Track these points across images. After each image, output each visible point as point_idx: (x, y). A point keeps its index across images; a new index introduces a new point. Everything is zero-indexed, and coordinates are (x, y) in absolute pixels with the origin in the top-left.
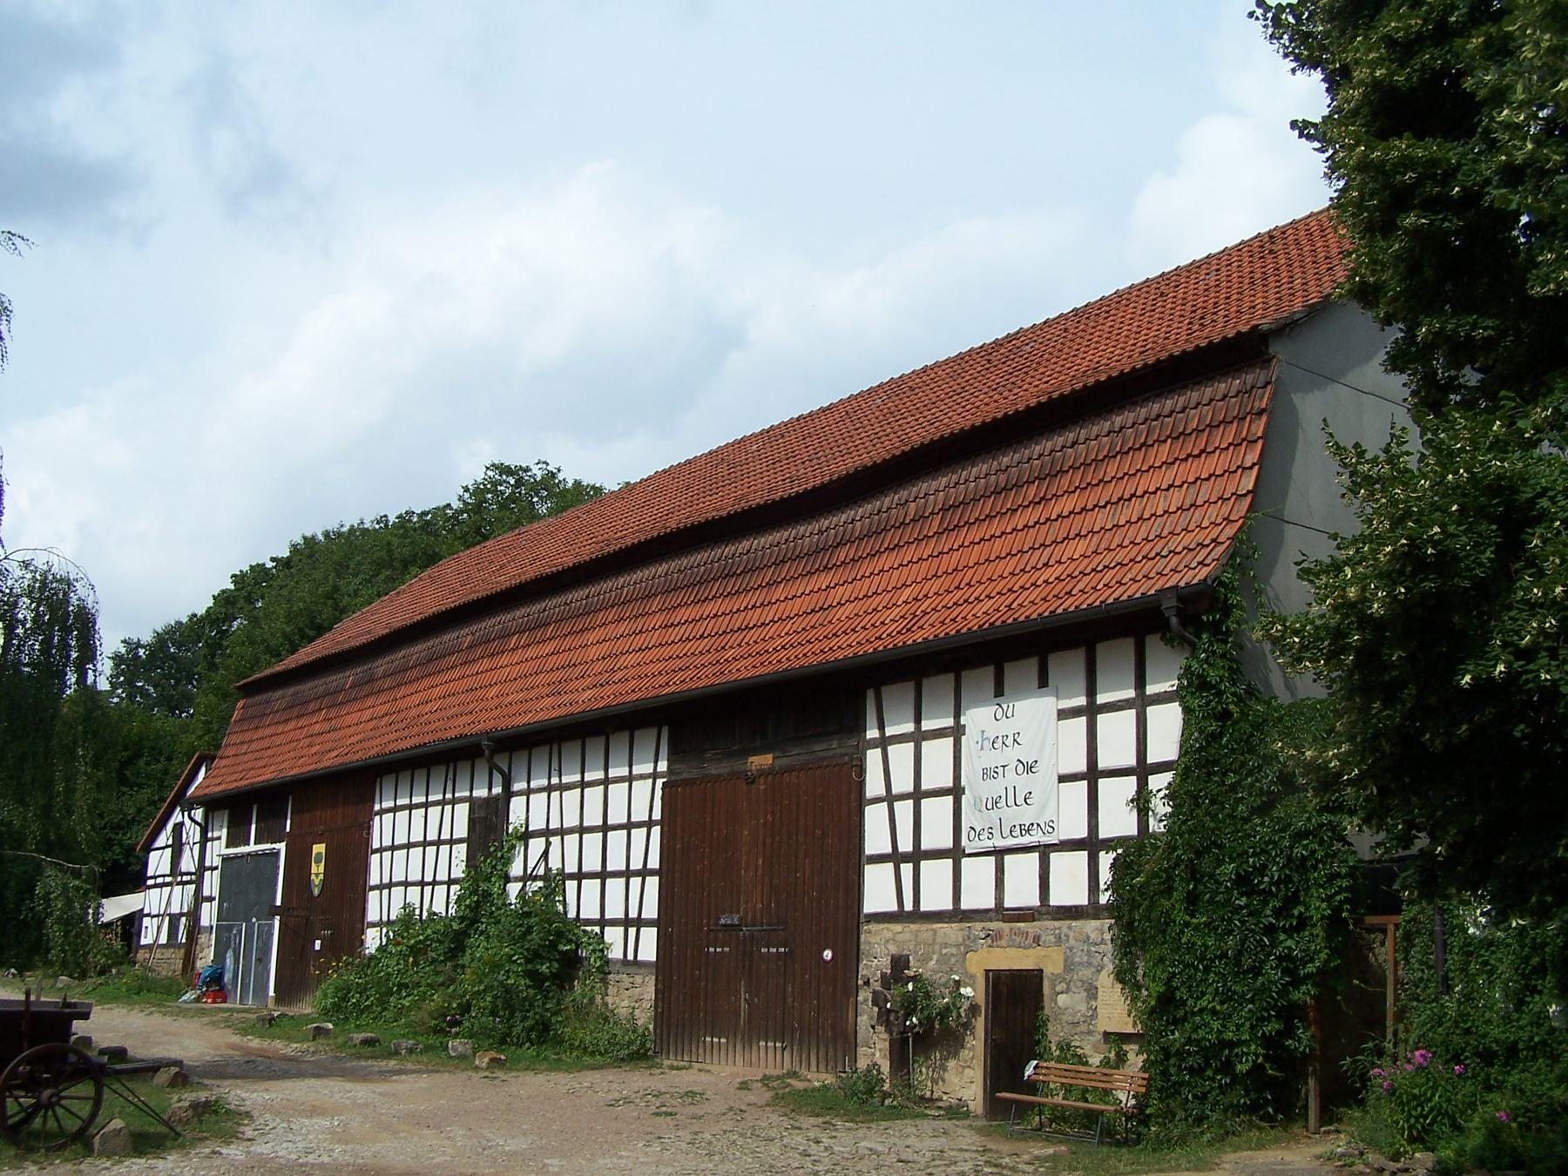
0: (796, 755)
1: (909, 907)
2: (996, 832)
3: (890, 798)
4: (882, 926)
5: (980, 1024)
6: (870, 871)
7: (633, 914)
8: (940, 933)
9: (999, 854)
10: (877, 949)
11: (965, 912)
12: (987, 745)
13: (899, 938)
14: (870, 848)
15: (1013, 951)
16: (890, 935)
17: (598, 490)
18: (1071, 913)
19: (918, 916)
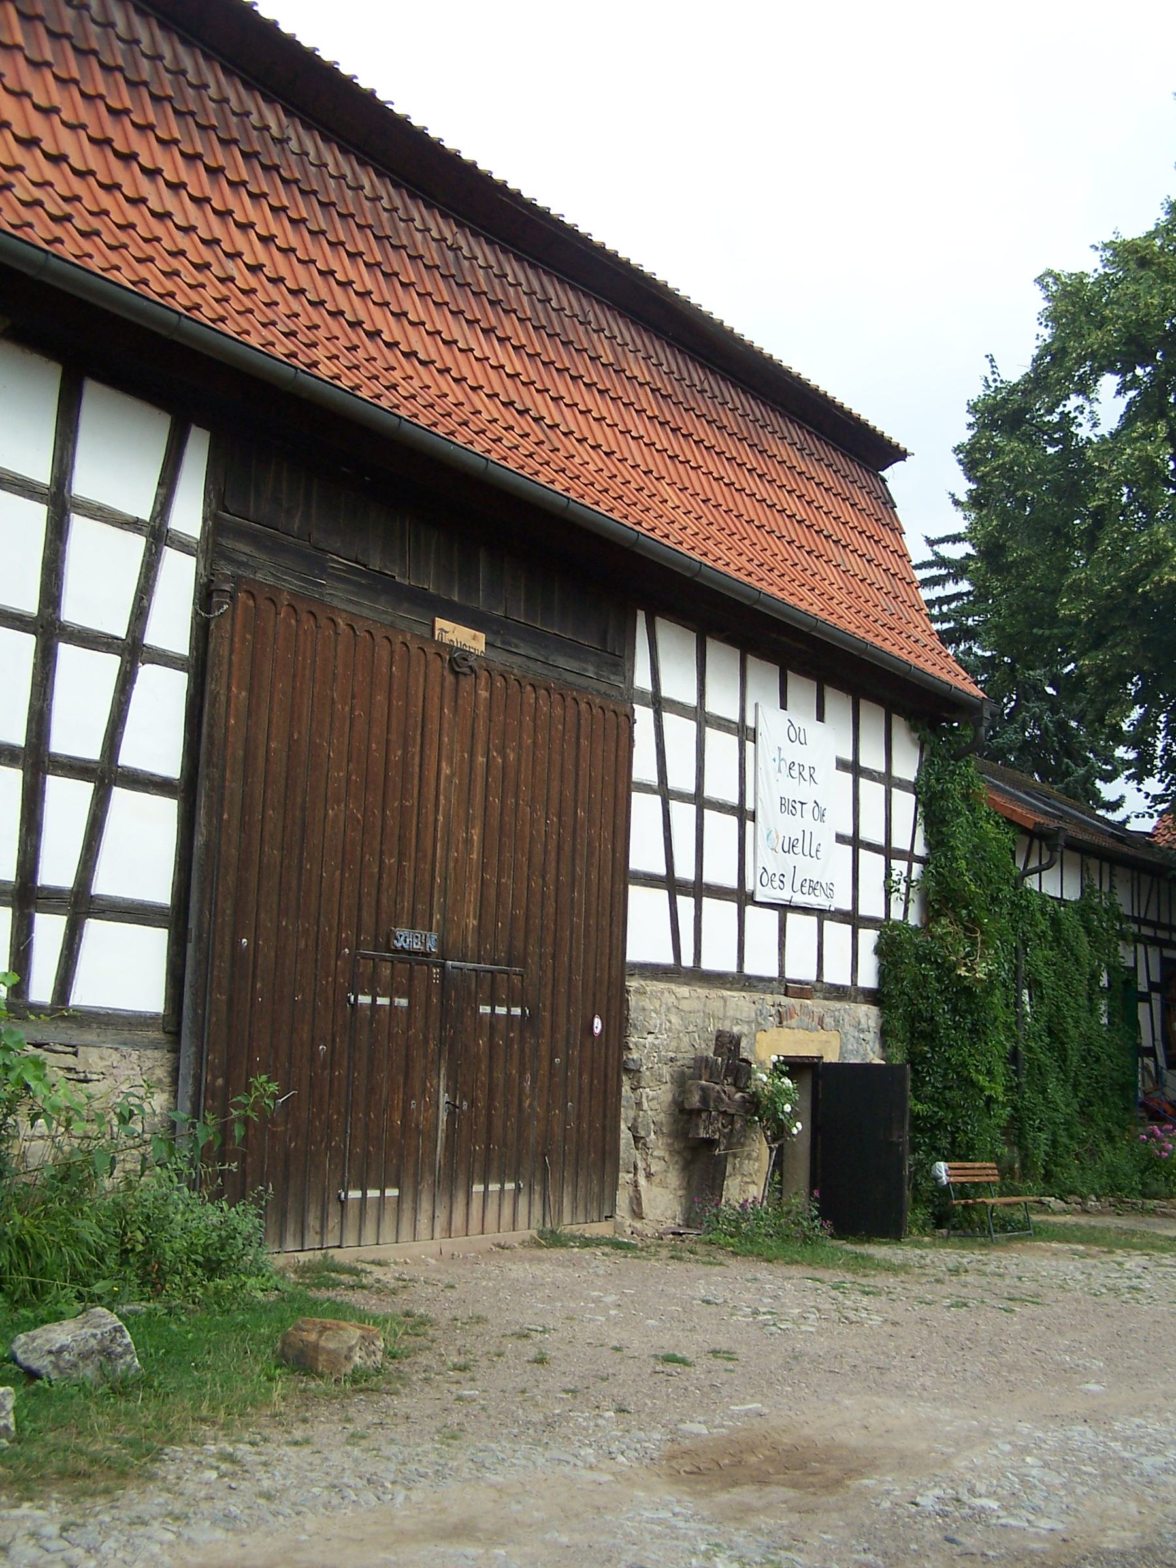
0: (518, 660)
1: (687, 960)
2: (788, 881)
3: (106, 775)
4: (661, 986)
5: (30, 1333)
6: (636, 893)
7: (57, 869)
8: (731, 1004)
9: (784, 909)
10: (655, 1020)
11: (749, 977)
12: (785, 770)
13: (685, 1005)
14: (637, 862)
15: (800, 1034)
16: (671, 1000)
17: (1045, 350)
18: (838, 993)
19: (699, 976)
